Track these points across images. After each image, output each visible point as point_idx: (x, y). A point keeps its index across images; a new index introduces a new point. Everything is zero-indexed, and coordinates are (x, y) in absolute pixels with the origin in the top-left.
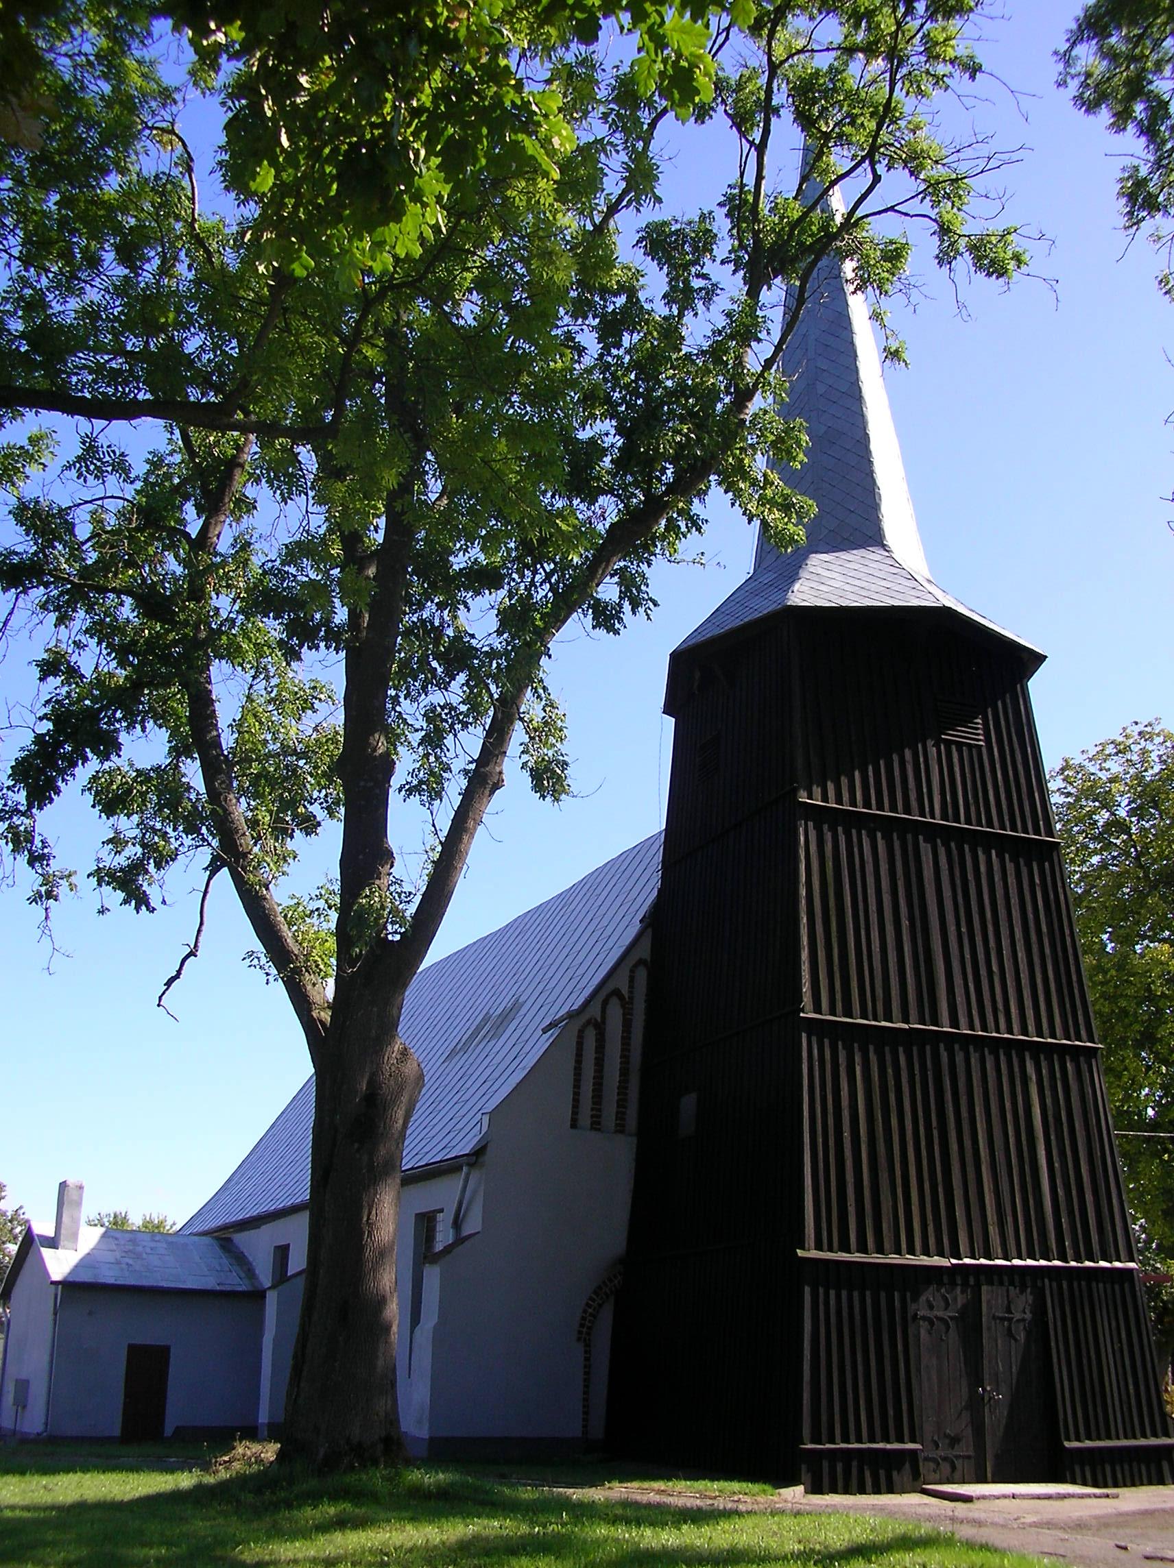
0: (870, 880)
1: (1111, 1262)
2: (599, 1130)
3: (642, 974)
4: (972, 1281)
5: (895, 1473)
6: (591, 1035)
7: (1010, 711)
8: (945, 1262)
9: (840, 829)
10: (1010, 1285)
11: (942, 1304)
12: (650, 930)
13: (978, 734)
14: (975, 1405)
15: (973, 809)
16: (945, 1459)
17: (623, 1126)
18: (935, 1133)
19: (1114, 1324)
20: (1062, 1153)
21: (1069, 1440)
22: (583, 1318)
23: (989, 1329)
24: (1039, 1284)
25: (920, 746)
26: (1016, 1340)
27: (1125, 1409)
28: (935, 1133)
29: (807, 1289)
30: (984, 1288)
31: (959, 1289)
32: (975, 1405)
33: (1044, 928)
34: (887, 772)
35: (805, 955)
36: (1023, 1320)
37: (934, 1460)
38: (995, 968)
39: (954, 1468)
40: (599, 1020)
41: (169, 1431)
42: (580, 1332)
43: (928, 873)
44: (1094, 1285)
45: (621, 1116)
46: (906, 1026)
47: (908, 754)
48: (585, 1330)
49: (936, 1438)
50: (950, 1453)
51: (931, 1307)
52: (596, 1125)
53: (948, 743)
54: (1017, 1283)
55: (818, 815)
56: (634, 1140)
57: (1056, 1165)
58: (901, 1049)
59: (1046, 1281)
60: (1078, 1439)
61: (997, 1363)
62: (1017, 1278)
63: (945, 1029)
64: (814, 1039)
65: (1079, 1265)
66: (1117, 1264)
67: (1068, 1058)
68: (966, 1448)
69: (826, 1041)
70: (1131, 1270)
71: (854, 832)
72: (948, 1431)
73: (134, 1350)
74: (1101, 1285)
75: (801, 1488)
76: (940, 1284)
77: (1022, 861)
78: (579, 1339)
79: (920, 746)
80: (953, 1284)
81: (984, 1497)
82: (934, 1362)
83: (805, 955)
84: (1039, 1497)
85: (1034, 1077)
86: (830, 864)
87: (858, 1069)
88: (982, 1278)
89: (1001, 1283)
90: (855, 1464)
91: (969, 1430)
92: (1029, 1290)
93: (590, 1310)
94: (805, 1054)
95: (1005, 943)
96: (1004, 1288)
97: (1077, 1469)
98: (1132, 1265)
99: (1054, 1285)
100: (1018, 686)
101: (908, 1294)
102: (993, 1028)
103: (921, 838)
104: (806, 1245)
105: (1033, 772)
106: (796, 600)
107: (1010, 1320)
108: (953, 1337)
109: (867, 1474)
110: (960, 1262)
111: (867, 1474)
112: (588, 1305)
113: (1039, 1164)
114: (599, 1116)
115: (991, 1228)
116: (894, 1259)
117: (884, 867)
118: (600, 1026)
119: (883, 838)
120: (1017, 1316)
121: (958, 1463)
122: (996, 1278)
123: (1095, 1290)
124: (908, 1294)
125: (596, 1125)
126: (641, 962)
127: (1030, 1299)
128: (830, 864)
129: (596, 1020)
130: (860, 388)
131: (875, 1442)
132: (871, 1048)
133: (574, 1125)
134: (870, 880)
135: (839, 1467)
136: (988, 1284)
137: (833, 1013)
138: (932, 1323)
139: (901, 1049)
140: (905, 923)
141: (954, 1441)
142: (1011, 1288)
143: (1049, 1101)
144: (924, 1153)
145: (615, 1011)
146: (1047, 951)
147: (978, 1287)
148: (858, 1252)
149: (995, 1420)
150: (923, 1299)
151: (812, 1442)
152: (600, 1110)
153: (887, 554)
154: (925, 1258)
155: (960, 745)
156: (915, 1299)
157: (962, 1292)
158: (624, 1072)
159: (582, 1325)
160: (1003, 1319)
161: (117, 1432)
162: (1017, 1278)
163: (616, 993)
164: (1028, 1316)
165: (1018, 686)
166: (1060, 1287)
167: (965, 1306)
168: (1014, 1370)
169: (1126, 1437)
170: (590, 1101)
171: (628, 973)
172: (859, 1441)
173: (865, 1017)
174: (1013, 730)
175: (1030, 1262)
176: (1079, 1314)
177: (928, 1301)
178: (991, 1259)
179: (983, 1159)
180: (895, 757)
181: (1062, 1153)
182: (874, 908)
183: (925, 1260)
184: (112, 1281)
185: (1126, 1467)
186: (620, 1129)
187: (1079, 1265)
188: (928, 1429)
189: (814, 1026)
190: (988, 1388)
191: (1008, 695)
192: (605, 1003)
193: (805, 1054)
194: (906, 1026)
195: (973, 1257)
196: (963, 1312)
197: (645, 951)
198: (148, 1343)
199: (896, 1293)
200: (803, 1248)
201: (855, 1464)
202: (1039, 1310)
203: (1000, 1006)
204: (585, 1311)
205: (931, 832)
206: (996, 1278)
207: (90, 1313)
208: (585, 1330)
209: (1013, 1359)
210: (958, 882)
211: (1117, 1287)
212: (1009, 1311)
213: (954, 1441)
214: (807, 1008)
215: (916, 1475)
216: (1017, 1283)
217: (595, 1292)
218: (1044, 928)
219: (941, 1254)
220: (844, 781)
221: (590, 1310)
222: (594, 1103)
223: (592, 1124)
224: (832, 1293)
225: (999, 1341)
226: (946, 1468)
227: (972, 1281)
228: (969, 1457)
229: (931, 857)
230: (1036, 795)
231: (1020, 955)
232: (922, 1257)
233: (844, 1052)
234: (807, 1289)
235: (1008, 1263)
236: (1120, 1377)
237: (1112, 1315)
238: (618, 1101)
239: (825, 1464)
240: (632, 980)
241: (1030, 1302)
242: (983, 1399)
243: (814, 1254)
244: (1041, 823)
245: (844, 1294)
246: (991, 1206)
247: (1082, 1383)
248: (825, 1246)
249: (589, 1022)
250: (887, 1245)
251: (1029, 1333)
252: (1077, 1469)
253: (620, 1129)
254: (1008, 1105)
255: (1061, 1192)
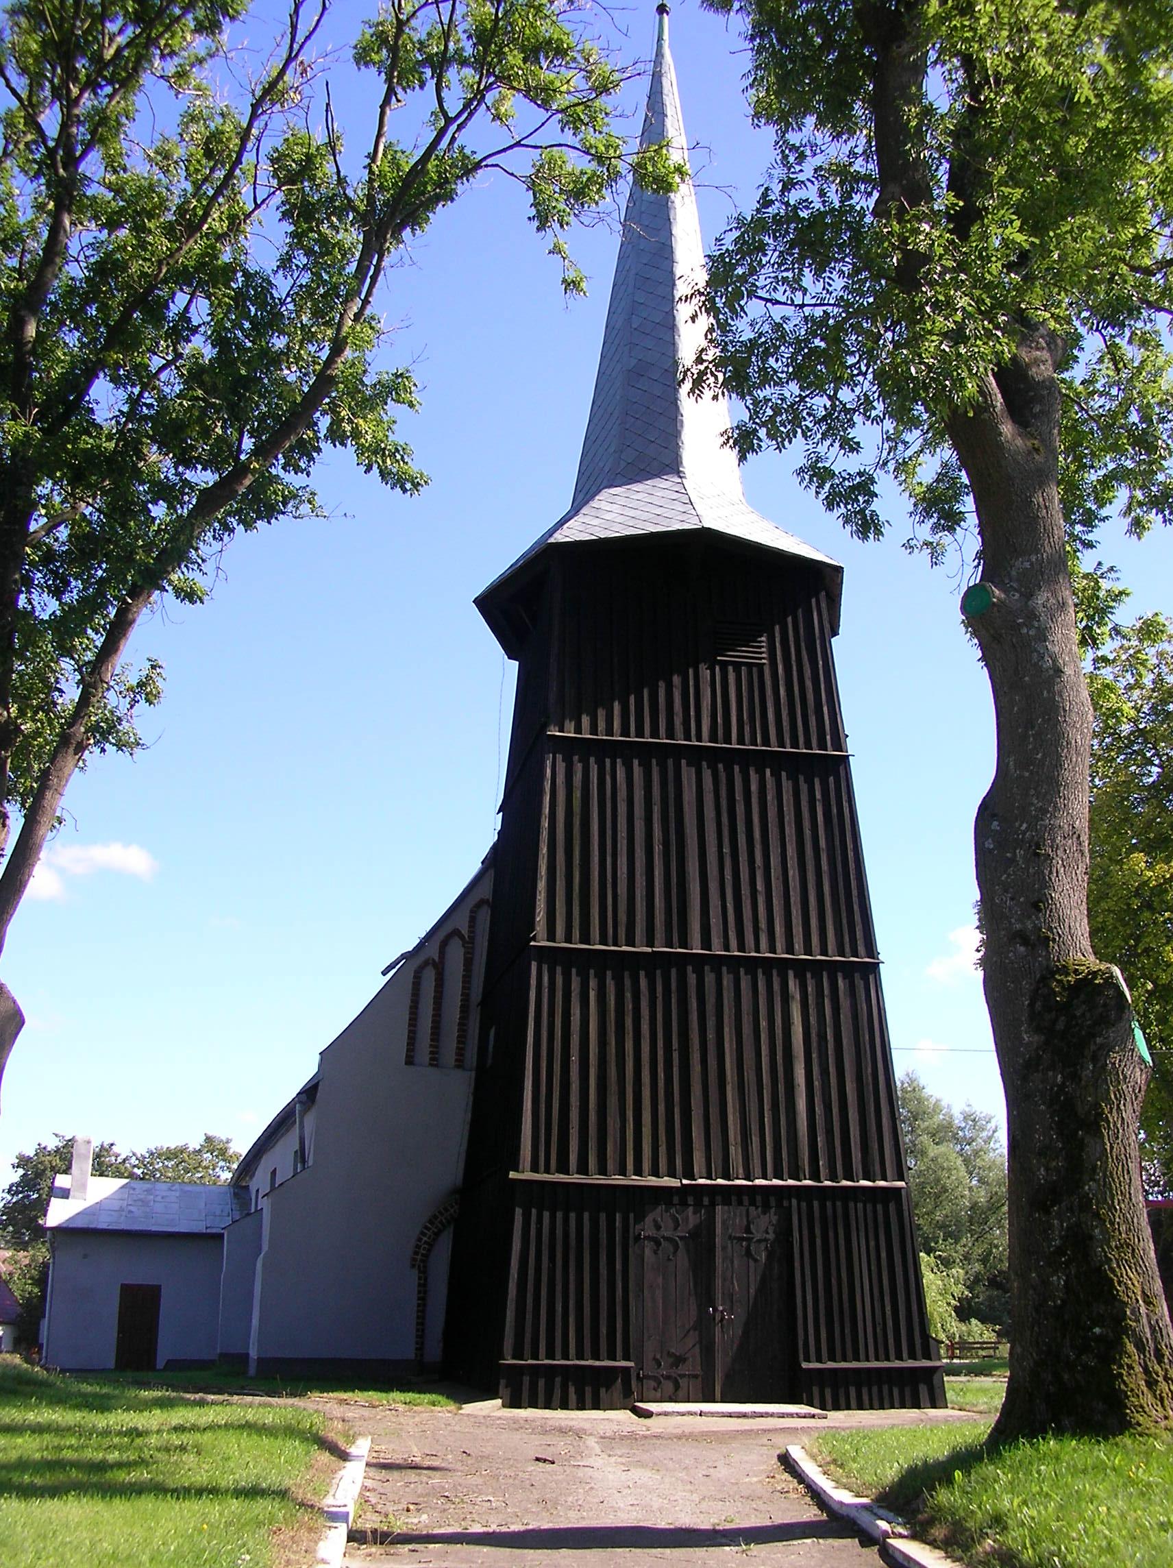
0: (622, 808)
1: (874, 1181)
2: (436, 1066)
3: (485, 916)
4: (706, 1201)
5: (603, 1390)
6: (429, 976)
7: (801, 625)
8: (674, 1183)
9: (592, 760)
10: (750, 1205)
11: (671, 1224)
12: (492, 872)
13: (761, 653)
14: (704, 1325)
15: (747, 729)
16: (668, 1378)
17: (462, 1061)
18: (676, 1055)
19: (872, 1243)
20: (825, 1072)
21: (808, 1360)
22: (418, 1247)
23: (724, 1248)
24: (785, 1203)
25: (691, 671)
26: (756, 1261)
27: (878, 1330)
28: (676, 1055)
29: (518, 1212)
30: (719, 1208)
31: (691, 1209)
32: (704, 1325)
33: (823, 843)
34: (650, 700)
35: (542, 885)
36: (766, 1240)
37: (655, 1378)
38: (760, 886)
39: (677, 1387)
40: (437, 959)
41: (160, 1364)
42: (414, 1260)
43: (689, 796)
44: (851, 1205)
45: (460, 1052)
46: (649, 950)
47: (676, 680)
48: (419, 1257)
49: (658, 1357)
50: (673, 1372)
51: (658, 1227)
52: (435, 1061)
53: (724, 665)
54: (759, 1203)
55: (568, 747)
56: (473, 1074)
57: (816, 1083)
58: (642, 974)
59: (794, 1202)
60: (819, 1360)
61: (733, 1283)
62: (759, 1198)
63: (694, 951)
64: (545, 968)
65: (834, 1184)
66: (882, 1183)
67: (574, 971)
68: (693, 1365)
69: (559, 970)
70: (899, 1189)
71: (608, 761)
72: (673, 1350)
73: (127, 1290)
74: (860, 1205)
75: (499, 1401)
76: (670, 1204)
77: (801, 778)
78: (413, 1266)
79: (691, 671)
80: (684, 1204)
81: (666, 1414)
82: (660, 1280)
83: (542, 885)
84: (730, 1415)
85: (798, 997)
86: (577, 794)
87: (592, 994)
88: (719, 1199)
89: (740, 1203)
90: (558, 1380)
91: (697, 1349)
92: (773, 1210)
93: (425, 1239)
94: (533, 982)
95: (775, 861)
96: (743, 1209)
97: (816, 1390)
98: (901, 1184)
99: (804, 1204)
100: (814, 600)
101: (632, 1215)
102: (753, 946)
103: (683, 762)
104: (521, 1167)
105: (823, 686)
106: (560, 537)
107: (749, 1240)
108: (682, 1260)
109: (572, 1390)
110: (694, 1182)
111: (572, 1390)
112: (423, 1234)
113: (796, 1082)
114: (437, 1053)
115: (732, 1149)
116: (618, 1180)
117: (639, 794)
118: (439, 966)
119: (657, 764)
120: (758, 1236)
121: (681, 1381)
122: (734, 1198)
123: (852, 1212)
124: (632, 1215)
125: (435, 1061)
126: (481, 903)
127: (774, 1219)
128: (577, 794)
129: (433, 959)
130: (674, 317)
131: (583, 1359)
132: (609, 974)
133: (410, 1061)
134: (622, 808)
135: (541, 1383)
136: (724, 1204)
137: (569, 940)
138: (658, 1243)
139: (642, 974)
140: (657, 848)
141: (679, 1360)
142: (752, 1209)
143: (813, 1020)
144: (661, 1075)
145: (456, 953)
146: (825, 866)
147: (713, 1204)
148: (578, 1173)
149: (726, 1339)
150: (649, 1220)
151: (514, 1358)
152: (437, 1047)
153: (679, 480)
154: (654, 1178)
155: (737, 666)
156: (640, 1218)
157: (695, 1213)
158: (465, 1009)
159: (416, 1253)
160: (743, 1239)
161: (113, 1367)
162: (759, 1198)
163: (456, 933)
164: (771, 1236)
165: (814, 600)
166: (810, 1207)
167: (698, 1227)
168: (752, 1291)
169: (877, 1359)
170: (429, 1037)
171: (468, 914)
172: (566, 1357)
173: (605, 943)
174: (803, 644)
175: (776, 1182)
176: (831, 1234)
177: (655, 1221)
178: (729, 1180)
179: (729, 1078)
180: (662, 685)
181: (825, 1072)
182: (624, 835)
183: (653, 1181)
184: (104, 1226)
185: (875, 1389)
186: (460, 1064)
187: (834, 1184)
188: (650, 1348)
189: (549, 956)
190: (721, 1308)
191: (800, 610)
192: (444, 944)
193: (533, 982)
194: (649, 950)
195: (709, 1178)
196: (695, 1234)
197: (486, 891)
198: (140, 1283)
199: (618, 1215)
200: (517, 1170)
201: (558, 1380)
202: (784, 1233)
203: (763, 924)
204: (420, 1240)
205: (697, 756)
206: (734, 1198)
207: (85, 1256)
208: (419, 1257)
209: (752, 1278)
210: (724, 803)
211: (879, 1207)
212: (748, 1230)
213: (679, 1360)
214: (539, 937)
215: (627, 1393)
216: (759, 1203)
217: (431, 1222)
218: (823, 843)
219: (672, 1175)
220: (601, 714)
221: (425, 1239)
222: (432, 1040)
223: (431, 1059)
224: (546, 1214)
225: (736, 1262)
226: (668, 1386)
227: (706, 1201)
228: (696, 1377)
229: (694, 780)
230: (825, 709)
231: (791, 873)
232: (650, 1178)
233: (579, 979)
234: (518, 1212)
235: (750, 1183)
236: (876, 1302)
237: (871, 1235)
238: (458, 1036)
239: (526, 1379)
240: (473, 920)
241: (774, 1222)
242: (714, 1319)
243: (528, 1175)
244: (828, 737)
245: (559, 1215)
246: (735, 1125)
247: (829, 1308)
248: (542, 1168)
249: (426, 963)
250: (610, 1166)
251: (770, 1256)
252: (816, 1390)
253: (460, 1064)
254: (763, 1024)
255: (819, 1110)
